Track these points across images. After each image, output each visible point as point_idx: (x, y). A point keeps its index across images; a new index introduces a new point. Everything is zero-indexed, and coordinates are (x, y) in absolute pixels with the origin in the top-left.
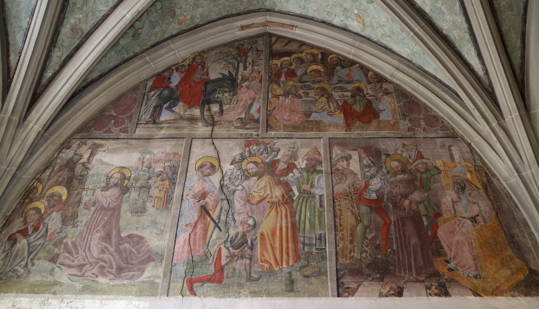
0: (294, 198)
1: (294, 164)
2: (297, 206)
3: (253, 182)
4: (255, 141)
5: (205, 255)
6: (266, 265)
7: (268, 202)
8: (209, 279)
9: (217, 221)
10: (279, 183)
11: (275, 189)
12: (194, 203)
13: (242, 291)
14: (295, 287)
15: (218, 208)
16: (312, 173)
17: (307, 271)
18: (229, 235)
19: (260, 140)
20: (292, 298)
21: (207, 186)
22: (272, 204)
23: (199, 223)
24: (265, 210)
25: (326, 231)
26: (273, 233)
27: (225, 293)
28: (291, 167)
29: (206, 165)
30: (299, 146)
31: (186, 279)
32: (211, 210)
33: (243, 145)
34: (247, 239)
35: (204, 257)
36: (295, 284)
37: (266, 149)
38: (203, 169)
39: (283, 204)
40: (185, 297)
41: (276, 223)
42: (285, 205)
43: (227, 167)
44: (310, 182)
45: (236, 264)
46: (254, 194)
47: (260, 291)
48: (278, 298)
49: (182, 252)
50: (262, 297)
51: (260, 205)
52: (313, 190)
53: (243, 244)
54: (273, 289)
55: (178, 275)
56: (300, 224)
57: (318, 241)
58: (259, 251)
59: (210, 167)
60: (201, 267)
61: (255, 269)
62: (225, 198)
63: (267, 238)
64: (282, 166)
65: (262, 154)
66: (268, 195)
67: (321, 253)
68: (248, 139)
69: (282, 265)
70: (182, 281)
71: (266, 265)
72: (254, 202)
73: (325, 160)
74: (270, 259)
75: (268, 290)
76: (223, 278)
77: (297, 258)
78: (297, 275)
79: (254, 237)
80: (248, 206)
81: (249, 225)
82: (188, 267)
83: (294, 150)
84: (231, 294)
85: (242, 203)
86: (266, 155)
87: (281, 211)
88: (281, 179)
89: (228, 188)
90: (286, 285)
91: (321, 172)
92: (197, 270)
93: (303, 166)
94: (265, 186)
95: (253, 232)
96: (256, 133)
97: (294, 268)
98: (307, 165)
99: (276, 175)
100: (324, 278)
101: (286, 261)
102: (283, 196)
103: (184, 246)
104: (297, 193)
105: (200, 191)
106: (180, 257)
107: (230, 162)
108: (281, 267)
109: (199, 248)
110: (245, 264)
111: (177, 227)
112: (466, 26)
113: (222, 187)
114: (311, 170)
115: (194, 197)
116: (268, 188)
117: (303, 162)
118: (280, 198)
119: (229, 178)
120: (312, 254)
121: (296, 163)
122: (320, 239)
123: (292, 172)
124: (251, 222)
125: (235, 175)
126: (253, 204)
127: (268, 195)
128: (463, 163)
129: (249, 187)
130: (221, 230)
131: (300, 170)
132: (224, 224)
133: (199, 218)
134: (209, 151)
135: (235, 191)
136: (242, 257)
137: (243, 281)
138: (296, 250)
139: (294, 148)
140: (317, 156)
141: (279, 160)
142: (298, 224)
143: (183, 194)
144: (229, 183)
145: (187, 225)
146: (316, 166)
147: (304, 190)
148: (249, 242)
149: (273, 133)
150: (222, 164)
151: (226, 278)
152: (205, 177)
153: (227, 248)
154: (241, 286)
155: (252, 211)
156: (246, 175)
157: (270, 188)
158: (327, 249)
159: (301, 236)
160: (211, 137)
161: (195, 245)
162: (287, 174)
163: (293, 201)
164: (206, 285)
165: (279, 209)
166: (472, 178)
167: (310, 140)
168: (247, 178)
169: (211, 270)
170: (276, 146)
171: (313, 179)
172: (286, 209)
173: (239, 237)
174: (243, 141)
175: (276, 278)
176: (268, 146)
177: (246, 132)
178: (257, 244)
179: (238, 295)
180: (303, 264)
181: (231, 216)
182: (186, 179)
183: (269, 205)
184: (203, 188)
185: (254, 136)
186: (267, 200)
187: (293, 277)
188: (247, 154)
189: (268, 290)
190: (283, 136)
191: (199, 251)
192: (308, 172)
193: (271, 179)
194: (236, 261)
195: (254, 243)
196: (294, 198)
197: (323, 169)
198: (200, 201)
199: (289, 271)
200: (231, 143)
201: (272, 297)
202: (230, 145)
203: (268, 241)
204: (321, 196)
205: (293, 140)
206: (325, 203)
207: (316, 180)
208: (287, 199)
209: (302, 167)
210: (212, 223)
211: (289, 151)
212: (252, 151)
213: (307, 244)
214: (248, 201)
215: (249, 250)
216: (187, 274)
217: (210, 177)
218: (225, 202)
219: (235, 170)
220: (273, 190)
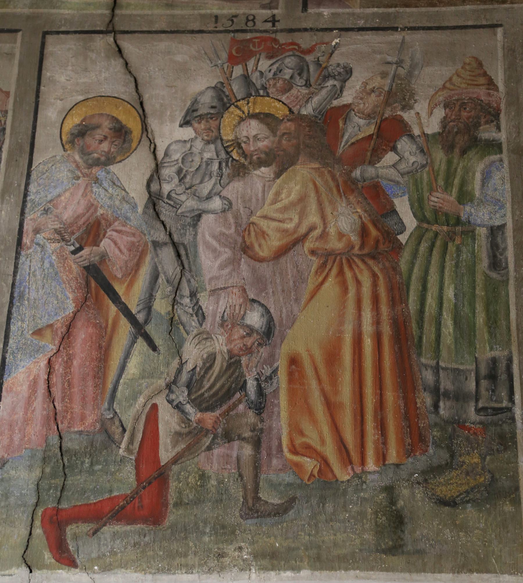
0: (403, 238)
1: (400, 121)
2: (413, 264)
3: (259, 186)
4: (263, 40)
5: (105, 430)
6: (310, 464)
7: (313, 252)
8: (120, 511)
9: (141, 317)
10: (349, 187)
11: (334, 209)
12: (62, 258)
13: (230, 549)
14: (407, 536)
15: (145, 272)
16: (464, 152)
17: (447, 483)
18: (182, 364)
19: (282, 38)
20: (397, 575)
21: (104, 198)
22: (327, 258)
23: (79, 324)
24: (300, 278)
25: (514, 349)
26: (332, 357)
27: (171, 555)
28: (389, 132)
29: (98, 127)
30: (418, 56)
31: (40, 512)
32: (121, 281)
33: (224, 55)
34: (242, 375)
35: (100, 438)
36: (408, 527)
37: (301, 69)
38: (88, 140)
39: (361, 257)
40: (37, 574)
41: (341, 323)
42: (371, 262)
43: (171, 134)
44: (457, 181)
45: (209, 459)
46: (264, 224)
47: (290, 550)
48: (352, 573)
49: (26, 421)
50: (296, 569)
51: (286, 261)
52: (466, 211)
53: (229, 394)
54: (335, 544)
55: (12, 500)
56: (421, 327)
57: (484, 383)
58: (284, 414)
59: (113, 133)
60: (91, 472)
61: (273, 476)
62: (167, 239)
63: (309, 371)
64: (358, 128)
65: (288, 87)
66: (312, 229)
67: (496, 424)
68: (240, 36)
69: (363, 462)
70: (25, 518)
71: (310, 464)
72: (264, 253)
73: (509, 104)
74: (323, 442)
75: (319, 547)
76: (166, 505)
77: (415, 439)
78: (413, 498)
79: (268, 371)
80: (243, 266)
81: (251, 330)
82: (48, 470)
83: (402, 72)
84: (191, 559)
85: (224, 257)
86: (304, 91)
87: (358, 283)
88: (357, 173)
89: (176, 206)
90: (379, 531)
91: (494, 146)
92: (76, 480)
93: (433, 127)
94: (302, 199)
95: (264, 351)
96: (267, 13)
97: (404, 474)
98: (444, 123)
99: (339, 161)
100: (508, 508)
101: (377, 449)
102: (364, 233)
103: (29, 401)
104: (410, 222)
105: (78, 217)
106: (17, 438)
107: (179, 117)
108: (358, 470)
109: (83, 407)
110: (238, 459)
111: (7, 337)
113: (154, 201)
114: (461, 141)
115: (61, 235)
116: (313, 206)
117: (431, 113)
118: (355, 239)
119: (179, 172)
120: (463, 426)
121: (408, 116)
122: (492, 377)
123: (394, 149)
124: (255, 318)
125: (197, 159)
126: (261, 260)
127: (312, 229)
129: (246, 201)
130: (154, 347)
131: (421, 141)
132: (165, 326)
133: (82, 305)
134: (105, 77)
135: (199, 216)
136: (228, 437)
137: (233, 516)
138: (409, 414)
139: (399, 63)
140: (481, 93)
141: (347, 107)
142: (414, 325)
143: (21, 225)
144: (180, 190)
145: (38, 332)
146: (477, 125)
147: (436, 212)
148: (251, 385)
149: (326, 12)
150: (153, 123)
151: (176, 505)
152: (95, 170)
153: (179, 407)
154: (225, 532)
155: (260, 282)
156: (238, 163)
157: (320, 203)
158: (518, 412)
159: (426, 366)
160: (110, 29)
161: (67, 396)
162: (376, 155)
163: (398, 247)
164: (107, 530)
165: (349, 275)
167: (458, 35)
168: (240, 171)
169: (125, 479)
170: (336, 59)
171: (467, 170)
172: (374, 276)
173: (217, 368)
174: (222, 43)
175: (345, 506)
176: (309, 58)
177: (233, 11)
178: (276, 392)
179: (217, 561)
180: (436, 462)
181: (187, 301)
182: (29, 175)
183: (315, 262)
184: (91, 206)
185: (260, 25)
186: (308, 245)
187: (401, 503)
188: (237, 88)
189: (319, 547)
190: (361, 23)
191: (83, 418)
192: (449, 148)
193: (321, 175)
194: (209, 448)
195: (269, 390)
196: (403, 238)
197: (503, 136)
198: (80, 249)
199: (386, 482)
200: (183, 50)
201: (332, 568)
202: (179, 58)
203: (314, 384)
204: (495, 232)
205: (397, 37)
206: (510, 254)
207: (478, 176)
208: (377, 242)
209: (429, 131)
210: (124, 321)
211: (384, 75)
212: (255, 77)
213: (447, 395)
214: (246, 249)
215: (251, 413)
216: (44, 496)
217: (114, 168)
218: (167, 254)
219: (199, 144)
220: (328, 210)
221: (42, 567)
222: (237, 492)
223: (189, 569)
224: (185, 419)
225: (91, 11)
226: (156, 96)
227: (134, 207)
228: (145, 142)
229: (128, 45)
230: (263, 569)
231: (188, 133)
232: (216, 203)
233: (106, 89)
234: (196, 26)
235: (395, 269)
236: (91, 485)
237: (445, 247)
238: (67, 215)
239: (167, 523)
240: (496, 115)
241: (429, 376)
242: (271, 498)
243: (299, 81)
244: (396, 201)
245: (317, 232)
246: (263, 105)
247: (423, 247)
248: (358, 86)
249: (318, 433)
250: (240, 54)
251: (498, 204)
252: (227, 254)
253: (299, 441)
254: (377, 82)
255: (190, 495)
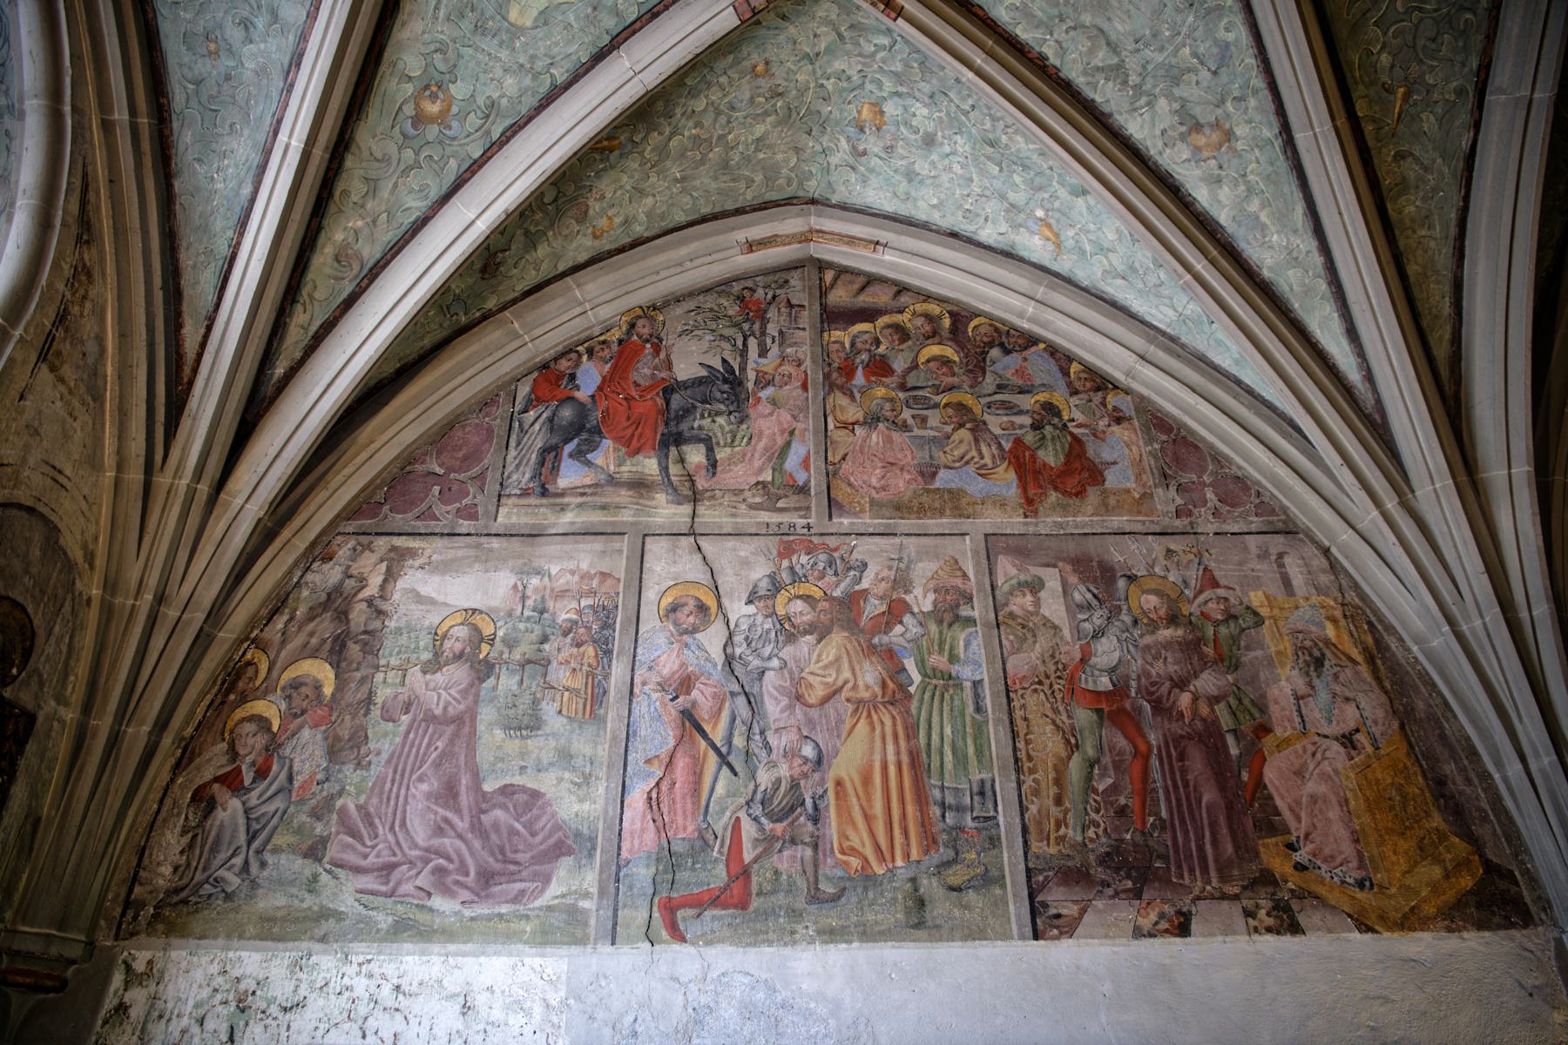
0: (912, 689)
6: (855, 862)
7: (848, 700)
8: (717, 900)
9: (724, 750)
10: (872, 650)
12: (664, 705)
13: (799, 928)
14: (927, 915)
16: (950, 625)
18: (756, 786)
19: (816, 540)
21: (692, 659)
23: (678, 755)
24: (840, 722)
26: (867, 780)
27: (756, 933)
28: (896, 611)
33: (775, 552)
35: (698, 843)
36: (928, 908)
37: (831, 563)
38: (679, 614)
39: (883, 704)
40: (657, 947)
41: (872, 754)
43: (739, 610)
44: (947, 647)
45: (780, 859)
46: (811, 678)
47: (843, 927)
49: (643, 830)
50: (849, 942)
52: (955, 669)
53: (792, 809)
56: (929, 756)
57: (976, 798)
58: (834, 824)
60: (693, 869)
63: (850, 791)
64: (874, 607)
65: (822, 576)
66: (846, 682)
68: (786, 538)
69: (893, 861)
70: (646, 904)
71: (855, 862)
72: (812, 700)
73: (979, 591)
74: (863, 845)
76: (750, 895)
77: (929, 842)
79: (820, 791)
81: (806, 760)
83: (902, 566)
86: (834, 579)
88: (876, 640)
89: (746, 665)
90: (908, 912)
91: (970, 621)
92: (683, 875)
93: (927, 606)
94: (838, 660)
95: (817, 776)
98: (935, 603)
99: (862, 631)
100: (998, 891)
102: (884, 686)
104: (917, 677)
107: (744, 597)
112: (1318, 260)
113: (729, 661)
114: (948, 617)
115: (662, 687)
116: (846, 665)
118: (878, 690)
121: (908, 598)
123: (901, 622)
124: (808, 751)
127: (846, 682)
128: (1315, 599)
131: (920, 617)
132: (743, 757)
133: (680, 741)
136: (793, 841)
137: (800, 903)
138: (924, 824)
139: (900, 560)
140: (959, 582)
145: (648, 761)
146: (958, 606)
147: (934, 670)
148: (809, 802)
149: (846, 521)
150: (726, 602)
152: (685, 637)
153: (756, 819)
154: (795, 914)
155: (810, 722)
156: (788, 632)
160: (692, 533)
161: (672, 811)
162: (889, 627)
163: (909, 696)
164: (708, 914)
165: (875, 717)
166: (1338, 637)
167: (939, 540)
168: (791, 638)
169: (719, 875)
170: (855, 555)
171: (953, 639)
172: (894, 718)
173: (783, 789)
174: (773, 543)
176: (836, 555)
178: (827, 807)
181: (757, 737)
183: (851, 707)
184: (683, 664)
186: (844, 694)
187: (922, 890)
190: (871, 530)
191: (685, 828)
192: (940, 622)
194: (780, 851)
196: (912, 689)
197: (976, 614)
198: (676, 697)
199: (911, 875)
200: (745, 548)
201: (875, 941)
202: (742, 554)
203: (854, 800)
204: (977, 684)
205: (897, 540)
206: (988, 701)
207: (962, 643)
210: (711, 753)
211: (890, 568)
212: (798, 568)
213: (950, 807)
214: (799, 697)
215: (809, 824)
216: (659, 887)
218: (741, 701)
219: (760, 618)
220: (857, 668)
221: (661, 942)
222: (802, 884)
223: (770, 943)
224: (762, 829)
225: (677, 519)
226: (727, 581)
227: (715, 665)
228: (721, 616)
229: (703, 542)
230: (825, 942)
231: (751, 609)
232: (775, 663)
233: (691, 577)
234: (753, 531)
235: (908, 712)
236: (692, 880)
237: (942, 696)
238: (666, 672)
239: (751, 908)
240: (971, 599)
241: (937, 794)
242: (828, 889)
243: (830, 572)
244: (905, 661)
245: (849, 685)
246: (804, 589)
247: (927, 695)
248: (872, 575)
249: (859, 838)
250: (786, 551)
251: (977, 664)
252: (785, 701)
253: (846, 844)
254: (885, 573)
255: (767, 887)
